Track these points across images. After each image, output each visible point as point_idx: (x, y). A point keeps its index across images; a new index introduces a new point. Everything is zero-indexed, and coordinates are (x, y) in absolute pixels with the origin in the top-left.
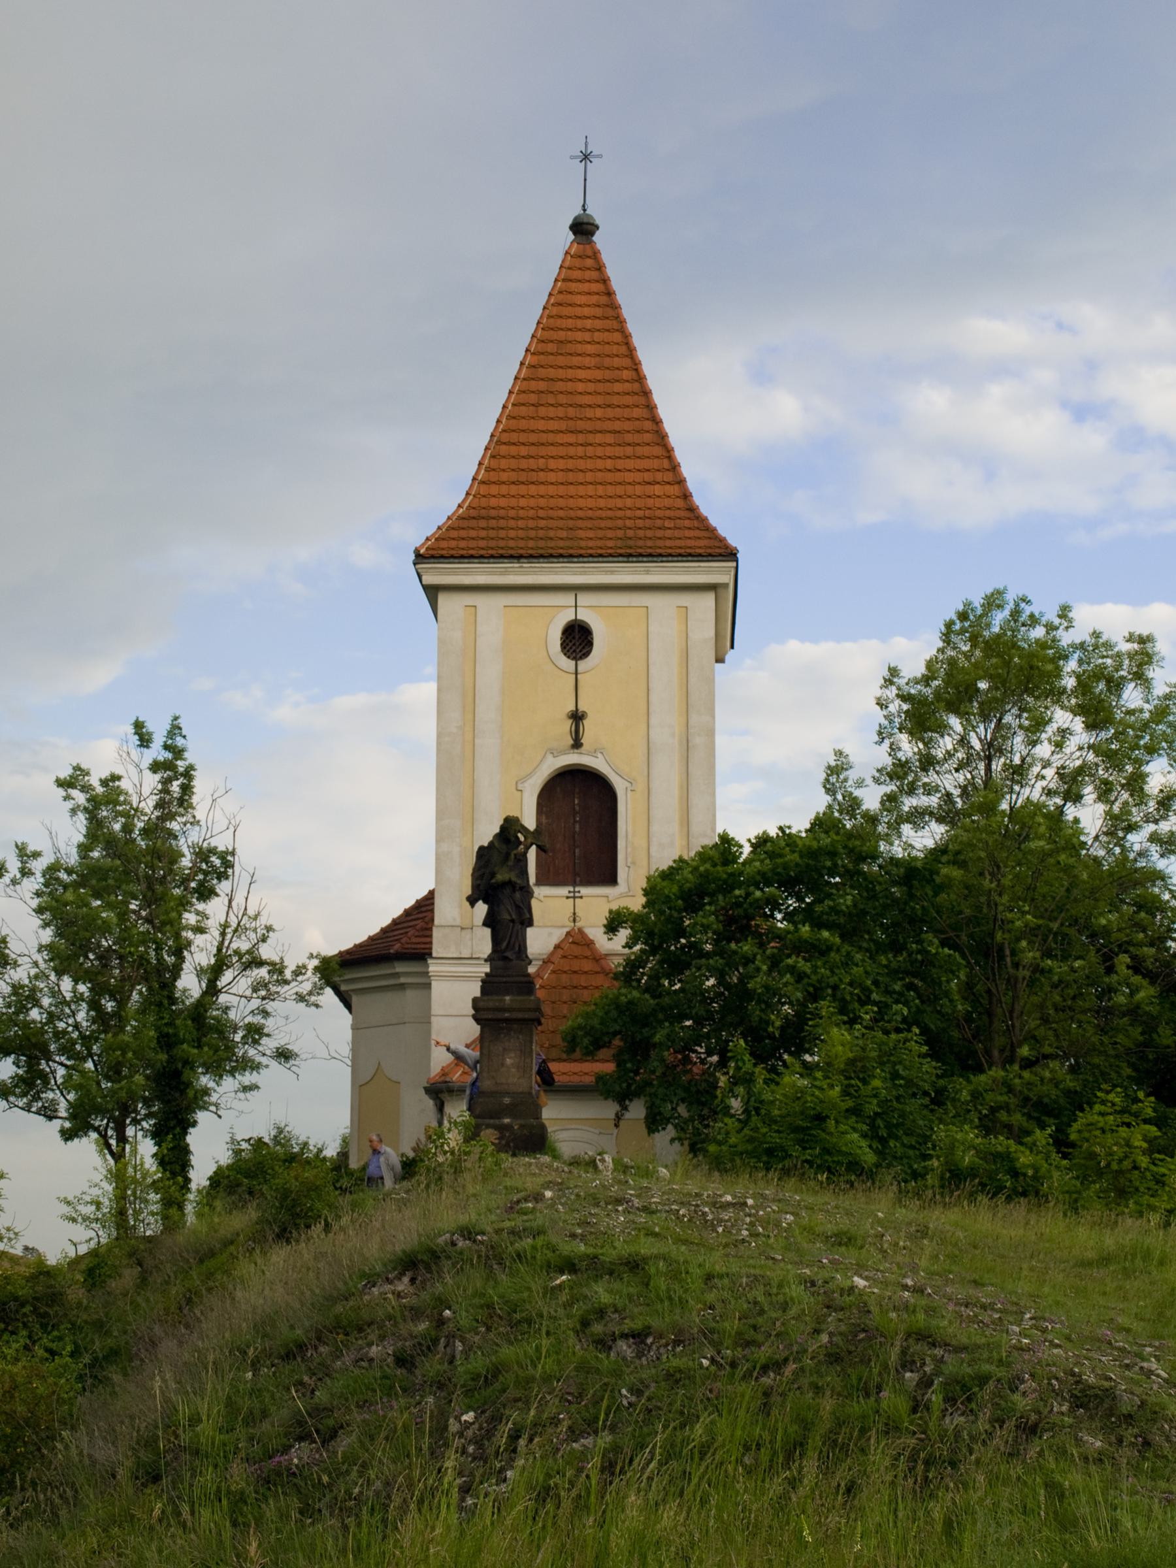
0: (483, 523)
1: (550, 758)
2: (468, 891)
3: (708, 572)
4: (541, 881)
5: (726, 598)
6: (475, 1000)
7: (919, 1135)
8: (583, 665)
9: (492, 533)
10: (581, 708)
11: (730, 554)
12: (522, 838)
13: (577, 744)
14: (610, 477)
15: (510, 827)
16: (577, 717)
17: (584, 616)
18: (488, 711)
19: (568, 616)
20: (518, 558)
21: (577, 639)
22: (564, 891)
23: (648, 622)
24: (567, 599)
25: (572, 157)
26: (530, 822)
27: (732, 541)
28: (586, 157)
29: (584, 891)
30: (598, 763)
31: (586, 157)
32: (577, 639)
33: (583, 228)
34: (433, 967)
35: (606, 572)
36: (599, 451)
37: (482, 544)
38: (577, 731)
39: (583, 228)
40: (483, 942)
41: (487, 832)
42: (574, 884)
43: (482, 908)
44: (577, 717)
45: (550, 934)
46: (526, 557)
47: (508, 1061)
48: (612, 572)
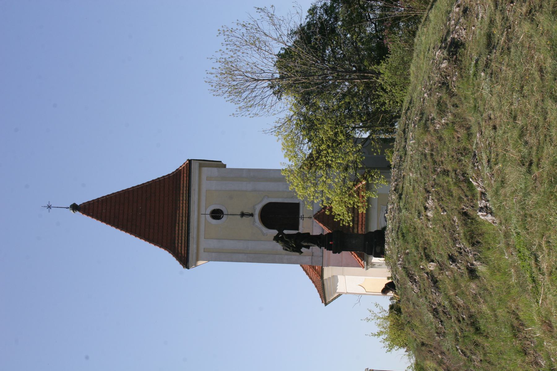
1: (257, 224)
2: (298, 254)
4: (297, 229)
5: (204, 163)
6: (334, 252)
8: (225, 212)
10: (239, 213)
12: (280, 236)
13: (252, 215)
15: (276, 239)
16: (243, 215)
17: (209, 211)
19: (209, 218)
20: (188, 234)
21: (217, 214)
22: (301, 221)
23: (203, 197)
24: (203, 217)
25: (49, 211)
26: (275, 232)
28: (49, 207)
29: (301, 214)
30: (259, 208)
31: (49, 207)
32: (217, 214)
33: (75, 207)
39: (75, 207)
41: (279, 246)
42: (298, 218)
43: (303, 250)
44: (243, 215)
45: (315, 226)
46: (309, 277)
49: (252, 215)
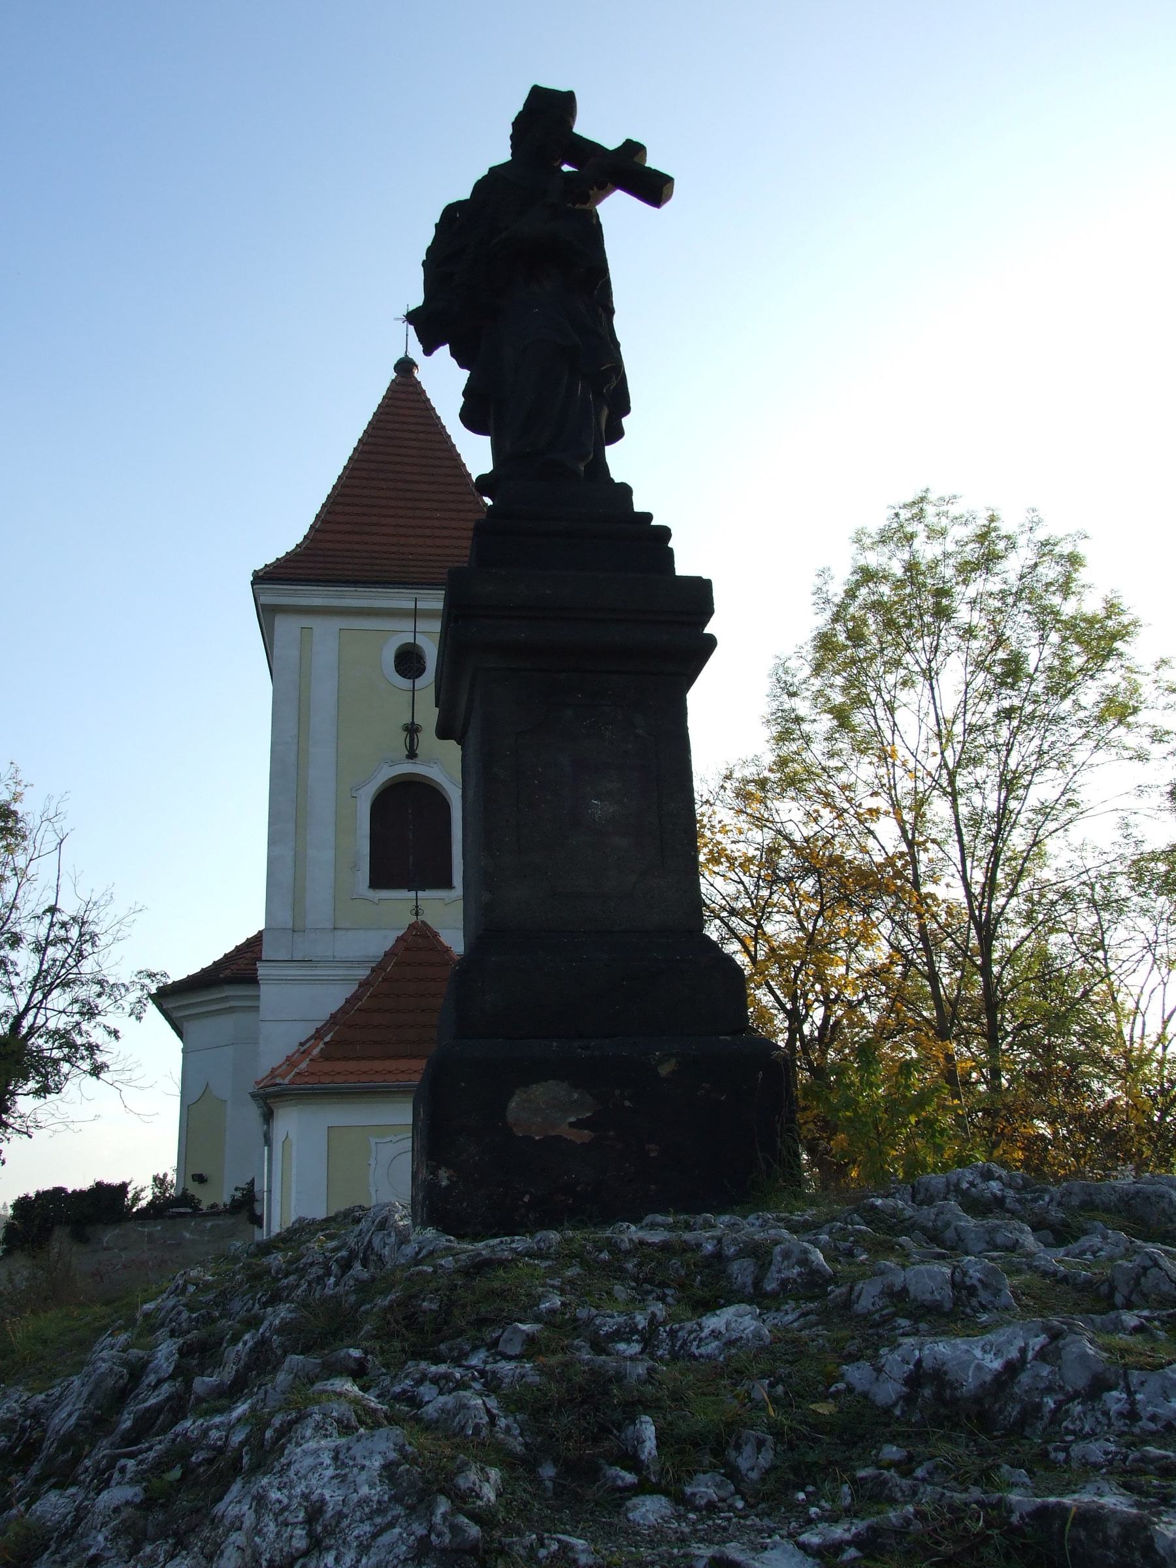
13: (412, 755)
38: (412, 741)
47: (599, 809)
49: (412, 755)
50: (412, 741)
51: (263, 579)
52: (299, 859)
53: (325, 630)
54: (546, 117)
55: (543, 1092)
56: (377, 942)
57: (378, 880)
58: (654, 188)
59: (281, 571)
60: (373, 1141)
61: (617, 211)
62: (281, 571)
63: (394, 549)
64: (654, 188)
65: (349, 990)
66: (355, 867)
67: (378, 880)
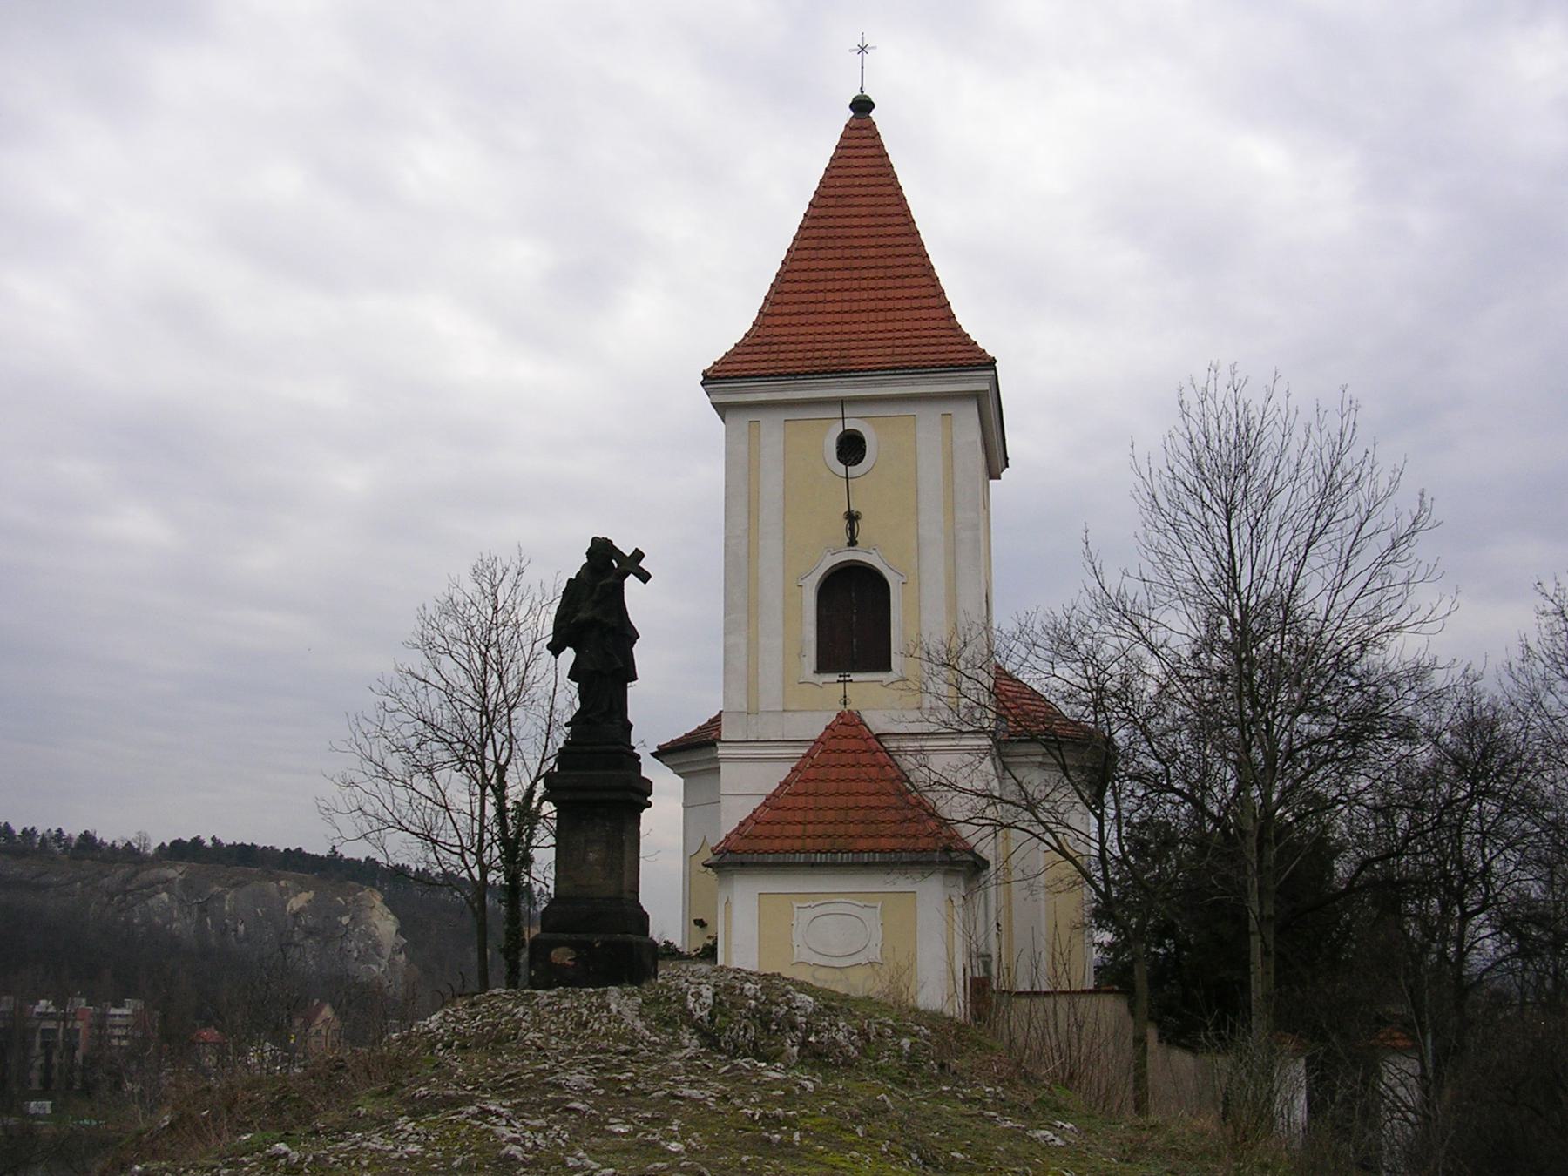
0: (766, 348)
3: (969, 381)
7: (852, 1146)
8: (854, 471)
9: (774, 356)
10: (854, 508)
11: (991, 363)
13: (853, 542)
14: (881, 305)
16: (852, 518)
18: (770, 514)
21: (851, 448)
22: (835, 677)
27: (990, 353)
29: (854, 677)
30: (873, 560)
32: (851, 448)
33: (862, 106)
34: (721, 751)
35: (876, 385)
36: (872, 284)
37: (764, 365)
38: (852, 529)
39: (862, 106)
40: (568, 699)
44: (852, 518)
47: (592, 856)
48: (881, 385)
49: (853, 542)
50: (852, 529)
51: (711, 379)
52: (753, 647)
53: (772, 427)
54: (601, 551)
55: (561, 950)
56: (813, 725)
57: (823, 666)
58: (644, 577)
59: (729, 367)
60: (796, 905)
61: (631, 582)
62: (729, 367)
63: (837, 328)
64: (644, 577)
65: (783, 771)
66: (801, 654)
67: (823, 666)
